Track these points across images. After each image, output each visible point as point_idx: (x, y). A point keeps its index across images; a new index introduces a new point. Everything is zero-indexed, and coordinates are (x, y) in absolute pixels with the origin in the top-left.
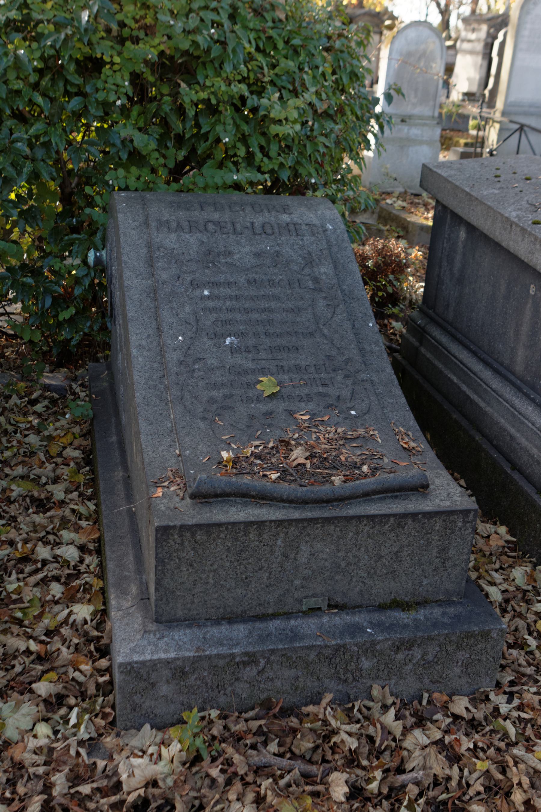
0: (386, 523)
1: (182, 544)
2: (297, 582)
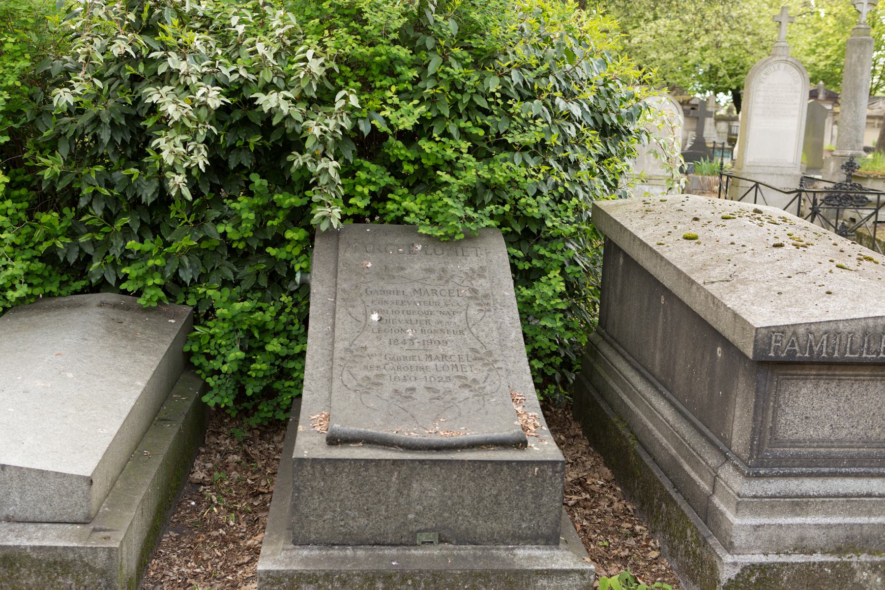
0: (485, 468)
1: (313, 475)
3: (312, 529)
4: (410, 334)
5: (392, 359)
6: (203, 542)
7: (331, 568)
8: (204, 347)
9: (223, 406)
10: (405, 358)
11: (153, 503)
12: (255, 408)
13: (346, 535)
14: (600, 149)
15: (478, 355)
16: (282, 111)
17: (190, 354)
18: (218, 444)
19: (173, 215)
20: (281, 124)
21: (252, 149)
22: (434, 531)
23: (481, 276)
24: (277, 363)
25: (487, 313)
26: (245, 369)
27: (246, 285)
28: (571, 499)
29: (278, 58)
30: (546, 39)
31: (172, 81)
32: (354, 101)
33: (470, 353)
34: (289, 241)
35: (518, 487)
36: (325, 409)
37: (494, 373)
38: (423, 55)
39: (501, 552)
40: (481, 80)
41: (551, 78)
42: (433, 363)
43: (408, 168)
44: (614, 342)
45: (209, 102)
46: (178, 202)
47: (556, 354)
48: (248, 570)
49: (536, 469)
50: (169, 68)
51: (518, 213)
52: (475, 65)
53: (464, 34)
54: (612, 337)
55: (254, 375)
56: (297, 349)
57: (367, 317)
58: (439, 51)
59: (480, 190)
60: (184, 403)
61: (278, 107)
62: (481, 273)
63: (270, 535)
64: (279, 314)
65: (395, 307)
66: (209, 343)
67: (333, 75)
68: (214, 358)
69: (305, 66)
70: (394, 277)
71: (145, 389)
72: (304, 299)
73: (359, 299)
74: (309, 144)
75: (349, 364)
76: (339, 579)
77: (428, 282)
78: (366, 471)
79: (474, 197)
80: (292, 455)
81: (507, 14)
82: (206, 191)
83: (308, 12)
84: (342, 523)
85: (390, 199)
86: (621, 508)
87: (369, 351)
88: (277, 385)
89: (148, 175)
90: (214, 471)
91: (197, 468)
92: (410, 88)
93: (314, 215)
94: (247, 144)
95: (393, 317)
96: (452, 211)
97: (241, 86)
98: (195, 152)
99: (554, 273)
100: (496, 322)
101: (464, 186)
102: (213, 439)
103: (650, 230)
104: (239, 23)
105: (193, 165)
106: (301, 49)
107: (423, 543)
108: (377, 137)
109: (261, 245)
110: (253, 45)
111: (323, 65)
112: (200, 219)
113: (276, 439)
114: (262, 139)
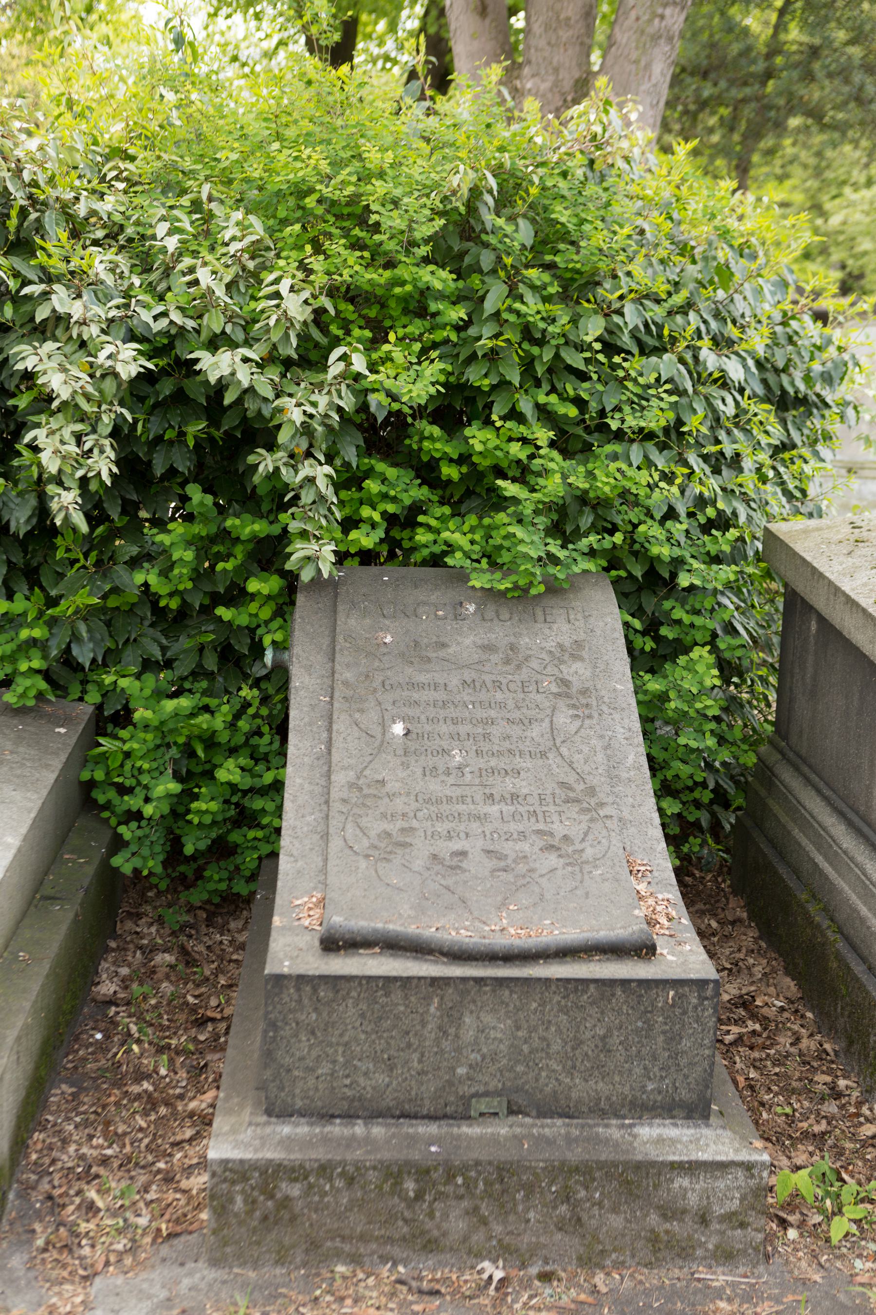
0: (585, 991)
1: (299, 1001)
2: (461, 1071)
3: (297, 1091)
4: (458, 758)
5: (428, 801)
6: (117, 1104)
7: (329, 1156)
8: (115, 773)
9: (145, 873)
10: (449, 799)
11: (34, 1042)
12: (199, 875)
13: (353, 1100)
14: (777, 433)
15: (572, 795)
16: (240, 382)
17: (91, 784)
18: (137, 933)
19: (60, 554)
20: (239, 401)
21: (191, 443)
22: (500, 1095)
23: (575, 657)
24: (234, 799)
25: (587, 722)
26: (181, 809)
27: (183, 668)
28: (728, 1032)
29: (234, 290)
30: (684, 249)
31: (59, 332)
32: (359, 364)
33: (557, 791)
34: (253, 596)
35: (640, 1024)
36: (318, 891)
37: (599, 825)
38: (475, 281)
39: (613, 1131)
40: (574, 321)
41: (692, 315)
42: (496, 808)
43: (449, 472)
44: (801, 763)
45: (119, 368)
46: (70, 537)
47: (704, 785)
48: (191, 1153)
49: (671, 993)
50: (54, 311)
51: (637, 547)
52: (564, 297)
53: (544, 242)
54: (799, 756)
55: (196, 821)
56: (268, 778)
57: (384, 728)
58: (502, 274)
59: (573, 509)
60: (82, 868)
61: (233, 374)
63: (227, 1099)
64: (237, 716)
65: (431, 712)
66: (122, 766)
67: (324, 318)
68: (129, 791)
69: (278, 306)
70: (429, 660)
71: (19, 850)
72: (278, 691)
73: (371, 698)
74: (283, 437)
75: (356, 810)
76: (343, 1174)
77: (486, 669)
78: (387, 995)
79: (561, 522)
80: (263, 969)
81: (616, 208)
82: (114, 514)
83: (282, 213)
84: (347, 1082)
85: (421, 525)
86: (813, 1048)
87: (390, 787)
88: (235, 837)
89: (20, 487)
90: (132, 981)
91: (104, 976)
92: (454, 337)
93: (291, 554)
94: (182, 434)
95: (428, 728)
96: (522, 548)
97: (172, 339)
98: (96, 451)
99: (701, 653)
101: (544, 503)
102: (129, 925)
103: (862, 577)
104: (170, 233)
105: (90, 474)
106: (271, 277)
107: (482, 1115)
108: (398, 422)
109: (207, 602)
110: (192, 270)
111: (306, 302)
112: (105, 558)
113: (233, 925)
114: (208, 426)
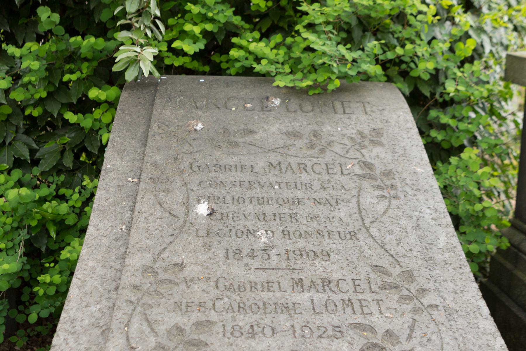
4: (263, 240)
5: (230, 288)
10: (253, 286)
15: (388, 280)
23: (375, 143)
25: (394, 202)
27: (45, 166)
33: (373, 276)
57: (188, 207)
62: (376, 138)
65: (237, 192)
70: (237, 145)
73: (178, 179)
75: (146, 299)
87: (187, 272)
95: (233, 208)
100: (411, 217)
